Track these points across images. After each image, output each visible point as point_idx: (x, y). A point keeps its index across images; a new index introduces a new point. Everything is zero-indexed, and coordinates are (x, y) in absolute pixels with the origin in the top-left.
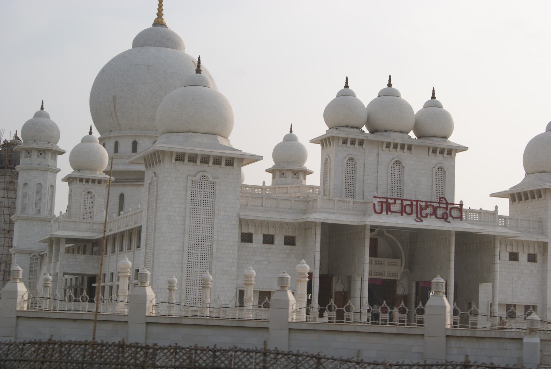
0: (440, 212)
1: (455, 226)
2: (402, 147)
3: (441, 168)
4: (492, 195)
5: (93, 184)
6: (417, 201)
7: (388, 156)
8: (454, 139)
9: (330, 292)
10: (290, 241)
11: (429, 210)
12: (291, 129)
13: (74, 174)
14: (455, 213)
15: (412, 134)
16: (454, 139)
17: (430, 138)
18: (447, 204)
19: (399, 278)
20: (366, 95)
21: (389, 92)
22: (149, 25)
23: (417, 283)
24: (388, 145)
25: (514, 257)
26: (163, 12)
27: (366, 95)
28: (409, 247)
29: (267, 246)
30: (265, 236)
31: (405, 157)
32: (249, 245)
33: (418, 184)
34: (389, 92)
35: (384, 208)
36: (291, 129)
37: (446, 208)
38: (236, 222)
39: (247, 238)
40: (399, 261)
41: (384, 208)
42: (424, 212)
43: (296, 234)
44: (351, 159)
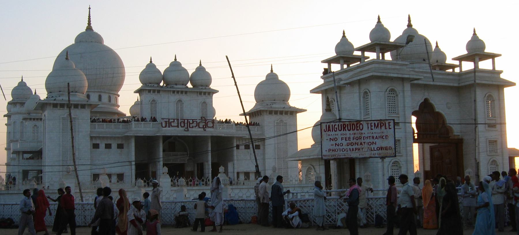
0: (201, 125)
1: (210, 132)
2: (182, 92)
3: (205, 102)
4: (306, 110)
5: (286, 115)
6: (188, 120)
7: (174, 98)
8: (212, 86)
9: (144, 171)
10: (120, 146)
11: (195, 124)
12: (272, 69)
13: (259, 107)
14: (210, 124)
15: (189, 85)
16: (212, 86)
17: (201, 86)
18: (206, 120)
19: (186, 162)
20: (162, 67)
21: (176, 65)
22: (84, 30)
23: (198, 164)
24: (174, 92)
25: (108, 146)
26: (91, 22)
27: (162, 67)
28: (192, 144)
29: (107, 150)
30: (106, 145)
31: (184, 98)
32: (98, 150)
33: (191, 110)
34: (176, 65)
35: (168, 125)
36: (272, 69)
37: (205, 123)
38: (88, 138)
39: (96, 146)
40: (186, 153)
41: (168, 125)
42: (191, 126)
43: (123, 142)
44: (154, 100)
